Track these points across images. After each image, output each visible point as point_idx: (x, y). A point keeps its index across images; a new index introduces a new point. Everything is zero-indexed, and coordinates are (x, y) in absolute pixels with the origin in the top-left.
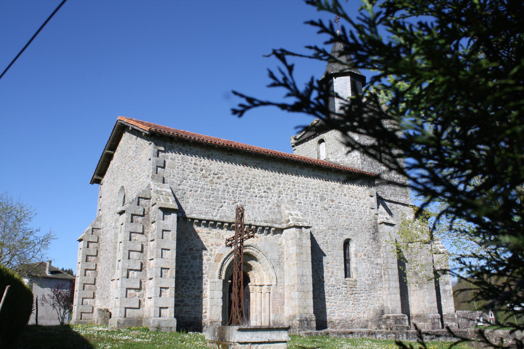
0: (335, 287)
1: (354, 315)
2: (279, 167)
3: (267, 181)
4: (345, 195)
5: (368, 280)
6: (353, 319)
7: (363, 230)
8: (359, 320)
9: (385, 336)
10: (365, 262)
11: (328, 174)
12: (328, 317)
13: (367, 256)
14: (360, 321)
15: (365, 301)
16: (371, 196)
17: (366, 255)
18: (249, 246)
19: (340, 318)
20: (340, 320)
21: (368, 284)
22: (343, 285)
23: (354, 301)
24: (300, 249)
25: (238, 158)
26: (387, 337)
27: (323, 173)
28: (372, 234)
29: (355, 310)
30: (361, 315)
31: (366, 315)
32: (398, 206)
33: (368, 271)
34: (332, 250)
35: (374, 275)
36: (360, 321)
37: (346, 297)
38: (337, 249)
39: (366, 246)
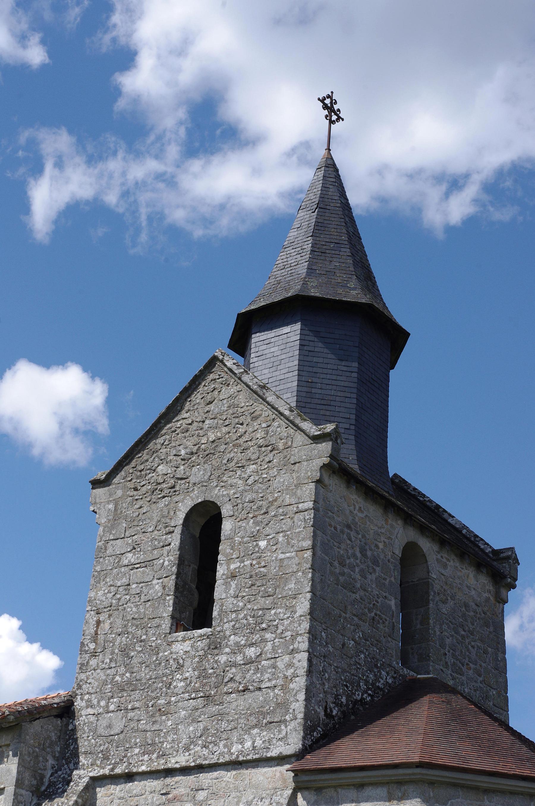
32: (205, 778)
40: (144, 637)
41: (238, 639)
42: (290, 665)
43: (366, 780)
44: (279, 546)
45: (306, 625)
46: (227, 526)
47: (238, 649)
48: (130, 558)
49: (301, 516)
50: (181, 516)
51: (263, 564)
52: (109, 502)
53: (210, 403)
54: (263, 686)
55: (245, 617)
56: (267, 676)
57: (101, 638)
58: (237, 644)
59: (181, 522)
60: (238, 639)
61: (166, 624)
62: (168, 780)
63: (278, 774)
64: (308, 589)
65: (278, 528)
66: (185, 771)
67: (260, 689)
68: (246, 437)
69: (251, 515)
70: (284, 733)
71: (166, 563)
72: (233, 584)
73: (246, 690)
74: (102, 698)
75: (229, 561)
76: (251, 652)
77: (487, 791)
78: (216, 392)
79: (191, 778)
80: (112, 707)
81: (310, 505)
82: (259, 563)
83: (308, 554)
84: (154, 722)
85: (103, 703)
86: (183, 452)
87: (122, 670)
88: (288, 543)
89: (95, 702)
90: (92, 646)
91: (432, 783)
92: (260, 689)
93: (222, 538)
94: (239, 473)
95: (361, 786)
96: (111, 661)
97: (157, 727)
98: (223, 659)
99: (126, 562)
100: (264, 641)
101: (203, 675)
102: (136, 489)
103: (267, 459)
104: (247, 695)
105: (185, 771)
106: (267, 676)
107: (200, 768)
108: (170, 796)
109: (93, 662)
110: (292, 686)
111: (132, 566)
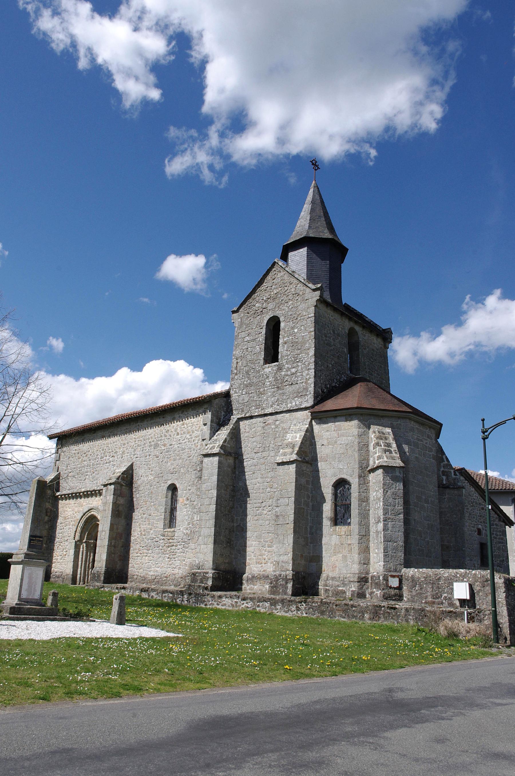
0: (154, 540)
1: (169, 571)
2: (125, 428)
3: (116, 445)
4: (178, 434)
5: (187, 529)
6: (167, 575)
7: (189, 469)
8: (174, 577)
9: (160, 594)
10: (186, 508)
11: (163, 418)
12: (52, 569)
13: (190, 500)
14: (175, 578)
15: (182, 554)
16: (205, 425)
17: (188, 500)
18: (92, 509)
19: (155, 573)
20: (156, 576)
21: (187, 534)
22: (161, 537)
23: (170, 554)
24: (104, 506)
25: (99, 433)
26: (162, 597)
27: (160, 418)
28: (199, 471)
29: (170, 565)
30: (176, 571)
31: (181, 572)
32: (279, 416)
33: (189, 518)
34: (155, 500)
35: (195, 523)
36: (175, 578)
37: (163, 551)
38: (160, 498)
39: (190, 488)
40: (254, 367)
41: (288, 366)
42: (308, 374)
43: (338, 415)
44: (302, 331)
45: (313, 359)
46: (282, 325)
47: (288, 369)
48: (247, 338)
49: (309, 319)
50: (265, 322)
51: (296, 338)
52: (239, 319)
53: (274, 279)
54: (298, 382)
55: (291, 358)
56: (299, 379)
57: (238, 368)
58: (288, 367)
59: (265, 324)
60: (288, 366)
61: (262, 362)
62: (265, 418)
63: (305, 414)
64: (314, 346)
65: (301, 324)
66: (271, 414)
67: (297, 384)
68: (288, 291)
69: (291, 320)
70: (307, 399)
71: (261, 340)
72: (286, 346)
73: (292, 384)
74: (240, 390)
75: (284, 337)
76: (293, 370)
77: (382, 417)
78: (276, 275)
79: (274, 417)
80: (244, 393)
81: (313, 315)
82: (295, 338)
83: (313, 333)
84: (259, 397)
85: (240, 392)
86: (265, 298)
87: (247, 379)
88: (305, 330)
89: (238, 391)
90: (235, 371)
91: (362, 415)
92: (297, 384)
93: (281, 329)
94: (286, 305)
95: (336, 417)
96: (242, 376)
97: (260, 399)
98: (283, 373)
99: (246, 340)
100: (298, 366)
101: (276, 380)
102: (248, 313)
103: (296, 299)
104: (293, 386)
105: (271, 414)
106: (299, 379)
107: (277, 413)
108: (266, 423)
109: (236, 377)
110: (309, 382)
111: (248, 342)
